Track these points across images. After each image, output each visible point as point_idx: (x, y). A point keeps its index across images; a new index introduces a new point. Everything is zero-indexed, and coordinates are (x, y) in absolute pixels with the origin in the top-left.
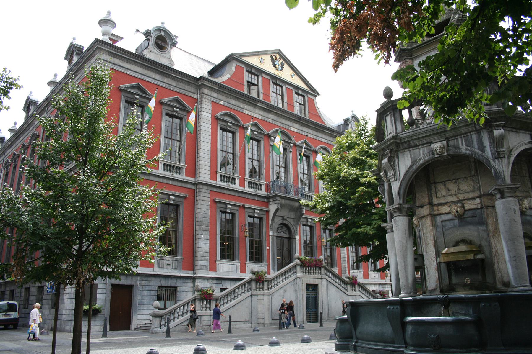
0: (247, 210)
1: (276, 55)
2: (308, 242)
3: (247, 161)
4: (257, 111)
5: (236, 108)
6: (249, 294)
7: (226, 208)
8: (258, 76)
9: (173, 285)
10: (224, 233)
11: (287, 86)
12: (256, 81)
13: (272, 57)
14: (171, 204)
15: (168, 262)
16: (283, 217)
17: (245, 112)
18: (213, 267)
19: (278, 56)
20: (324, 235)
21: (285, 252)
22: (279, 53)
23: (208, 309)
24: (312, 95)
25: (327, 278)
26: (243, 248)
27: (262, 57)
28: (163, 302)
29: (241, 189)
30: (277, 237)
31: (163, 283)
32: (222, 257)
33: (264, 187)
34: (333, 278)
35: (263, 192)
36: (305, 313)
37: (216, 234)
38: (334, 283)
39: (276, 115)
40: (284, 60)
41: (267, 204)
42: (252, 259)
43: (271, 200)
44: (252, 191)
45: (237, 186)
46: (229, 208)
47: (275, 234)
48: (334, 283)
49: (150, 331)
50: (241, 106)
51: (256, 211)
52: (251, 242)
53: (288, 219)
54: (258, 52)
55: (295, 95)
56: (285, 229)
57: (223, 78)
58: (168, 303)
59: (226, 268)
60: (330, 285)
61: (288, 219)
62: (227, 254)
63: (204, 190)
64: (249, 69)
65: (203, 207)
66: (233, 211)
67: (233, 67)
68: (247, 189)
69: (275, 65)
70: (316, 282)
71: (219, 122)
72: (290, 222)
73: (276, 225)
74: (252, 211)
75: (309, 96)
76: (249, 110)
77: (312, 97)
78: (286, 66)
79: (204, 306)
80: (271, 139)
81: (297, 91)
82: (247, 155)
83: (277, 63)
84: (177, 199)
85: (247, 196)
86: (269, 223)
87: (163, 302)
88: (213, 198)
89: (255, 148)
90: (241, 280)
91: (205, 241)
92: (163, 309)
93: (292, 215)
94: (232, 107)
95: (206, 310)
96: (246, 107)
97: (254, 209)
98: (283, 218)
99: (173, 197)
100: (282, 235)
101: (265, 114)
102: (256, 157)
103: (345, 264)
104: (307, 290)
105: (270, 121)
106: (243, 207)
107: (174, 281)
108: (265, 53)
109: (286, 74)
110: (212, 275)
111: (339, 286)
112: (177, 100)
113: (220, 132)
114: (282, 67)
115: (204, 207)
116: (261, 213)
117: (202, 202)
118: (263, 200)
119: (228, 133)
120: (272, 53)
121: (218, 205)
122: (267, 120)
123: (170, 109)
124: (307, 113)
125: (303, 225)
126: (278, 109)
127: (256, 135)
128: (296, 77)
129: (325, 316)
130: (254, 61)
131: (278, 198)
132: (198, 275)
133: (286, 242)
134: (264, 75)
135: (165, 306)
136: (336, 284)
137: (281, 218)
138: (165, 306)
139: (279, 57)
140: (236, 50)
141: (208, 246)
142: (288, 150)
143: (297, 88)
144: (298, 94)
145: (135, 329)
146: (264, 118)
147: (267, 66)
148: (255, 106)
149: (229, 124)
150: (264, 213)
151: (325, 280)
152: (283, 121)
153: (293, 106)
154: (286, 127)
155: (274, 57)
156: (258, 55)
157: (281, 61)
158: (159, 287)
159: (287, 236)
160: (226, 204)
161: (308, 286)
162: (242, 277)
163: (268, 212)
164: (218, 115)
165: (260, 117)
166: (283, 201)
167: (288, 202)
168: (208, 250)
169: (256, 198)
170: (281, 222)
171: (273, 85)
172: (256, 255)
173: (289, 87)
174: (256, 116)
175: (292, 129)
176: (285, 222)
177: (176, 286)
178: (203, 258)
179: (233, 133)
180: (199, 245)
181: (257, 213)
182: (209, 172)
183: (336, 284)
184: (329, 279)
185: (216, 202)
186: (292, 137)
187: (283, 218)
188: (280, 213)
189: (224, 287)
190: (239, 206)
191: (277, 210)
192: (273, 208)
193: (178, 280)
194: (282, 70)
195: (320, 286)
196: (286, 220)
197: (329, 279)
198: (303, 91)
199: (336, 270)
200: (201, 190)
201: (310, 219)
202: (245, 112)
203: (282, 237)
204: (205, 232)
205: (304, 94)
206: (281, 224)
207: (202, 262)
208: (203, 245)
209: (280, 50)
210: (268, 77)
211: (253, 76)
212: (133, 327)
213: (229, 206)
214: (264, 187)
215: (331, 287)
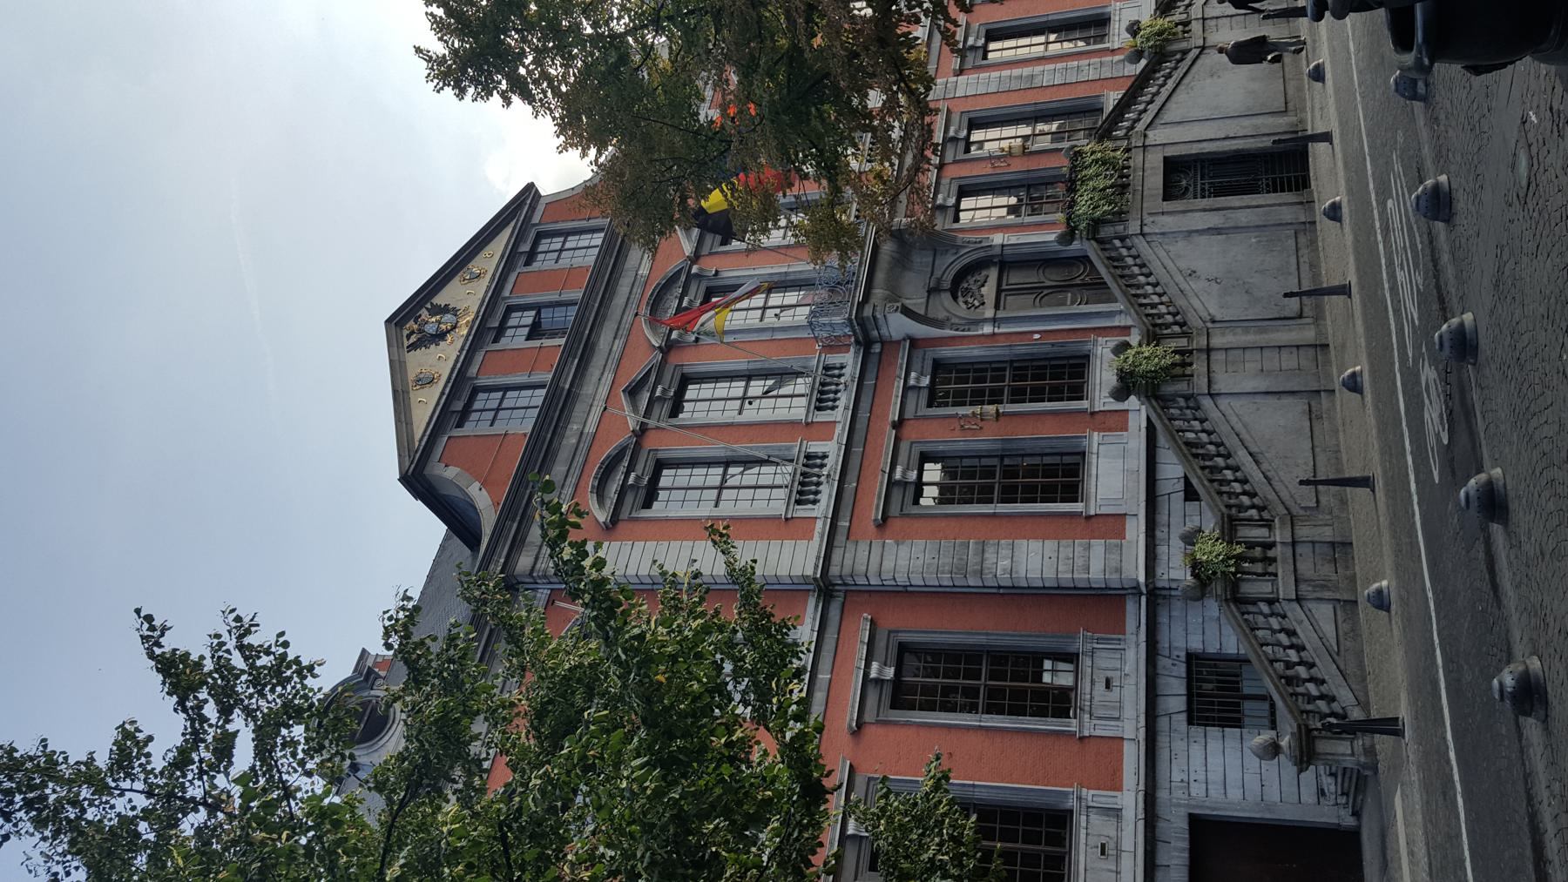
0: (909, 414)
1: (406, 332)
2: (1013, 200)
3: (750, 414)
4: (588, 389)
5: (580, 459)
6: (1207, 402)
7: (904, 484)
8: (476, 391)
9: (1182, 669)
10: (991, 489)
11: (506, 293)
12: (493, 395)
13: (413, 347)
14: (898, 673)
15: (1100, 687)
16: (929, 292)
17: (590, 428)
18: (1111, 525)
19: (412, 325)
20: (987, 146)
21: (1051, 277)
22: (396, 322)
23: (1271, 554)
24: (532, 208)
25: (1140, 126)
26: (1031, 424)
27: (411, 376)
28: (1247, 706)
29: (841, 432)
30: (997, 307)
31: (1175, 701)
32: (1072, 492)
33: (835, 359)
34: (1153, 90)
35: (849, 360)
36: (1272, 198)
37: (994, 515)
38: (1159, 100)
39: (602, 324)
40: (421, 305)
41: (889, 344)
42: (1077, 393)
43: (875, 333)
44: (845, 400)
45: (832, 449)
46: (904, 473)
47: (989, 313)
48: (1159, 100)
49: (1367, 773)
50: (574, 441)
51: (912, 382)
52: (1018, 396)
53: (938, 273)
54: (395, 392)
55: (536, 266)
56: (970, 282)
57: (485, 504)
58: (1247, 688)
59: (1113, 474)
60: (1168, 116)
61: (938, 273)
62: (1060, 477)
63: (848, 562)
64: (454, 419)
65: (903, 563)
66: (893, 652)
67: (447, 473)
68: (840, 415)
69: (440, 336)
70: (1155, 160)
71: (624, 515)
72: (948, 266)
73: (960, 310)
74: (911, 396)
75: (536, 219)
76: (587, 418)
77: (541, 208)
78: (440, 300)
79: (1259, 567)
80: (676, 341)
81: (523, 259)
82: (730, 413)
83: (431, 329)
84: (903, 457)
85: (863, 414)
86: (953, 338)
87: (1247, 706)
88: (872, 528)
89: (706, 390)
90: (1151, 428)
91: (1021, 555)
92: (1273, 706)
93: (921, 259)
94: (575, 472)
95: (1274, 560)
96: (575, 427)
97: (906, 388)
98: (933, 291)
99: (875, 665)
100: (989, 291)
101: (597, 361)
102: (737, 388)
103: (1089, 70)
104: (1183, 195)
105: (618, 344)
106: (898, 425)
107: (1163, 662)
108: (397, 368)
109: (467, 297)
110: (1136, 531)
111: (1171, 84)
112: (633, 392)
113: (658, 509)
114: (445, 310)
115: (907, 559)
116: (917, 364)
117: (888, 565)
118: (874, 359)
119: (663, 482)
120: (400, 345)
121: (894, 509)
122: (616, 354)
123: (629, 499)
124: (593, 223)
125: (957, 219)
126: (580, 318)
127: (664, 391)
128: (476, 266)
129: (1281, 123)
130: (425, 404)
131: (868, 311)
132: (1142, 579)
133: (1016, 278)
134: (473, 371)
135: (1262, 698)
136: (1165, 92)
137: (935, 300)
138: (1262, 698)
139: (412, 323)
140: (387, 461)
141: (1035, 545)
142: (712, 284)
143: (510, 261)
144: (531, 257)
145: (1356, 814)
146: (611, 365)
147: (441, 360)
148: (571, 398)
149: (631, 481)
150: (918, 353)
151: (1150, 133)
152: (619, 300)
153: (571, 268)
154: (638, 290)
155: (413, 339)
156: (406, 392)
157: (424, 313)
158: (1190, 722)
159: (993, 274)
160: (891, 483)
161: (1171, 192)
162: (1144, 424)
163: (914, 343)
164: (602, 516)
165: (608, 377)
166: (879, 292)
167: (880, 276)
168: (1050, 544)
169: (869, 382)
170: (946, 298)
171: (503, 341)
172: (1061, 374)
173: (509, 286)
174: (603, 392)
175: (644, 271)
176: (947, 285)
177: (1183, 654)
178: (1079, 562)
179: (660, 465)
180: (1034, 574)
181: (918, 379)
182: (788, 544)
183: (1165, 92)
184: (1147, 118)
185: (885, 518)
186: (671, 268)
187: (933, 291)
188: (917, 302)
189: (1181, 486)
190: (897, 440)
191: (907, 312)
192: (898, 326)
193: (1164, 644)
194: (455, 311)
195: (1171, 152)
196: (939, 280)
197: (1147, 118)
198: (519, 238)
199: (1111, 98)
200: (847, 571)
201: (946, 131)
202: (646, 272)
203: (999, 291)
204: (990, 556)
205: (532, 235)
206: (955, 298)
207: (1095, 562)
208: (1032, 558)
209: (388, 322)
210: (479, 357)
211: (477, 405)
212: (1349, 821)
213: (898, 475)
214: (835, 359)
215: (1173, 112)
